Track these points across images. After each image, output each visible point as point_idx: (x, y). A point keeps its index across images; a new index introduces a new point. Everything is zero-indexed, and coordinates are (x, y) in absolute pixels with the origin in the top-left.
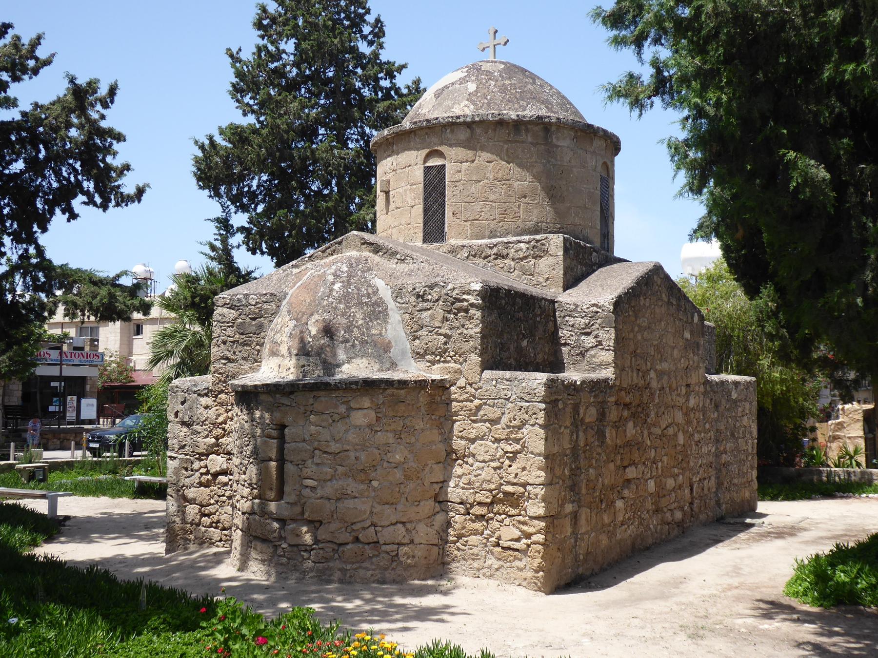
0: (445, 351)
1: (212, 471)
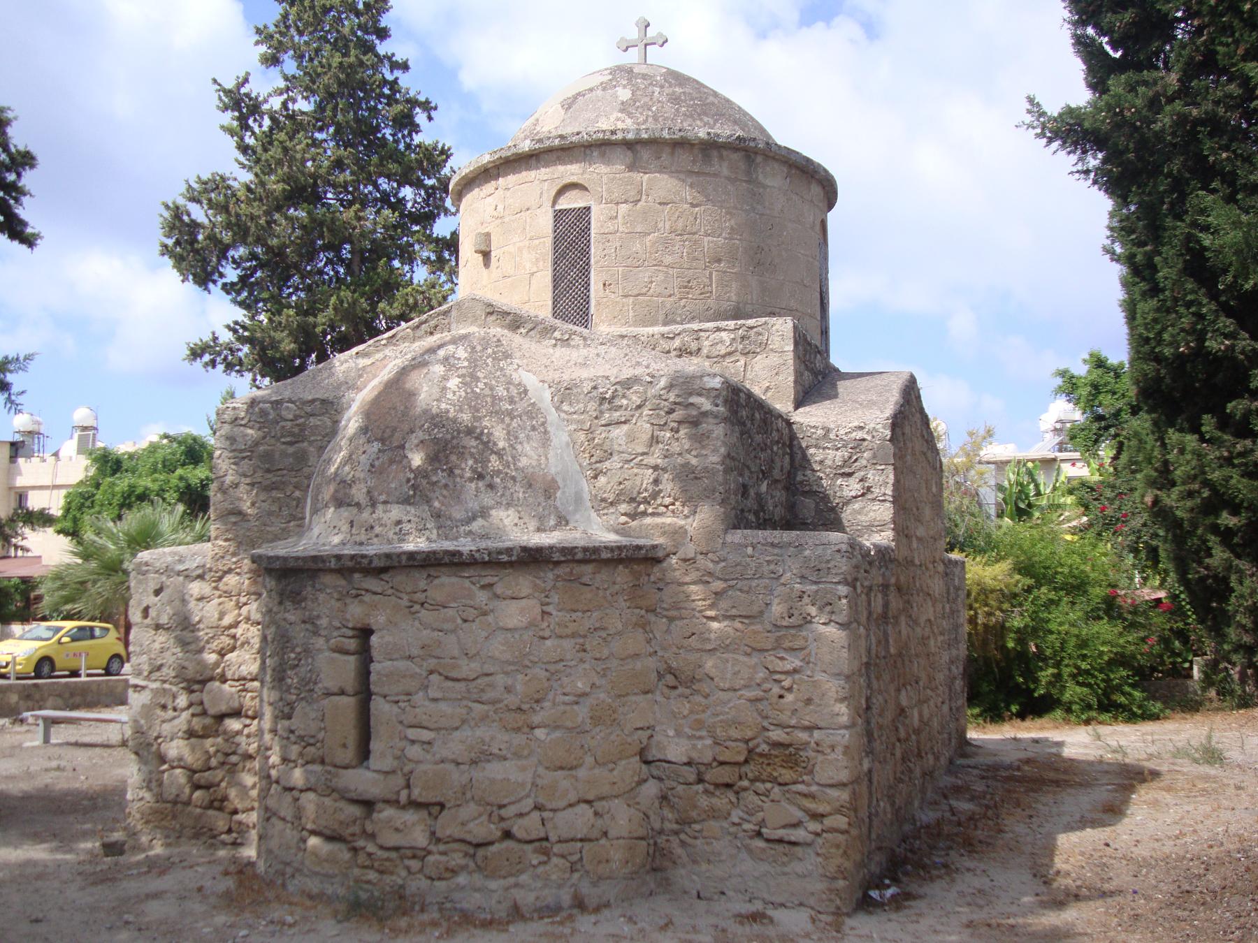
0: (655, 495)
1: (212, 711)
